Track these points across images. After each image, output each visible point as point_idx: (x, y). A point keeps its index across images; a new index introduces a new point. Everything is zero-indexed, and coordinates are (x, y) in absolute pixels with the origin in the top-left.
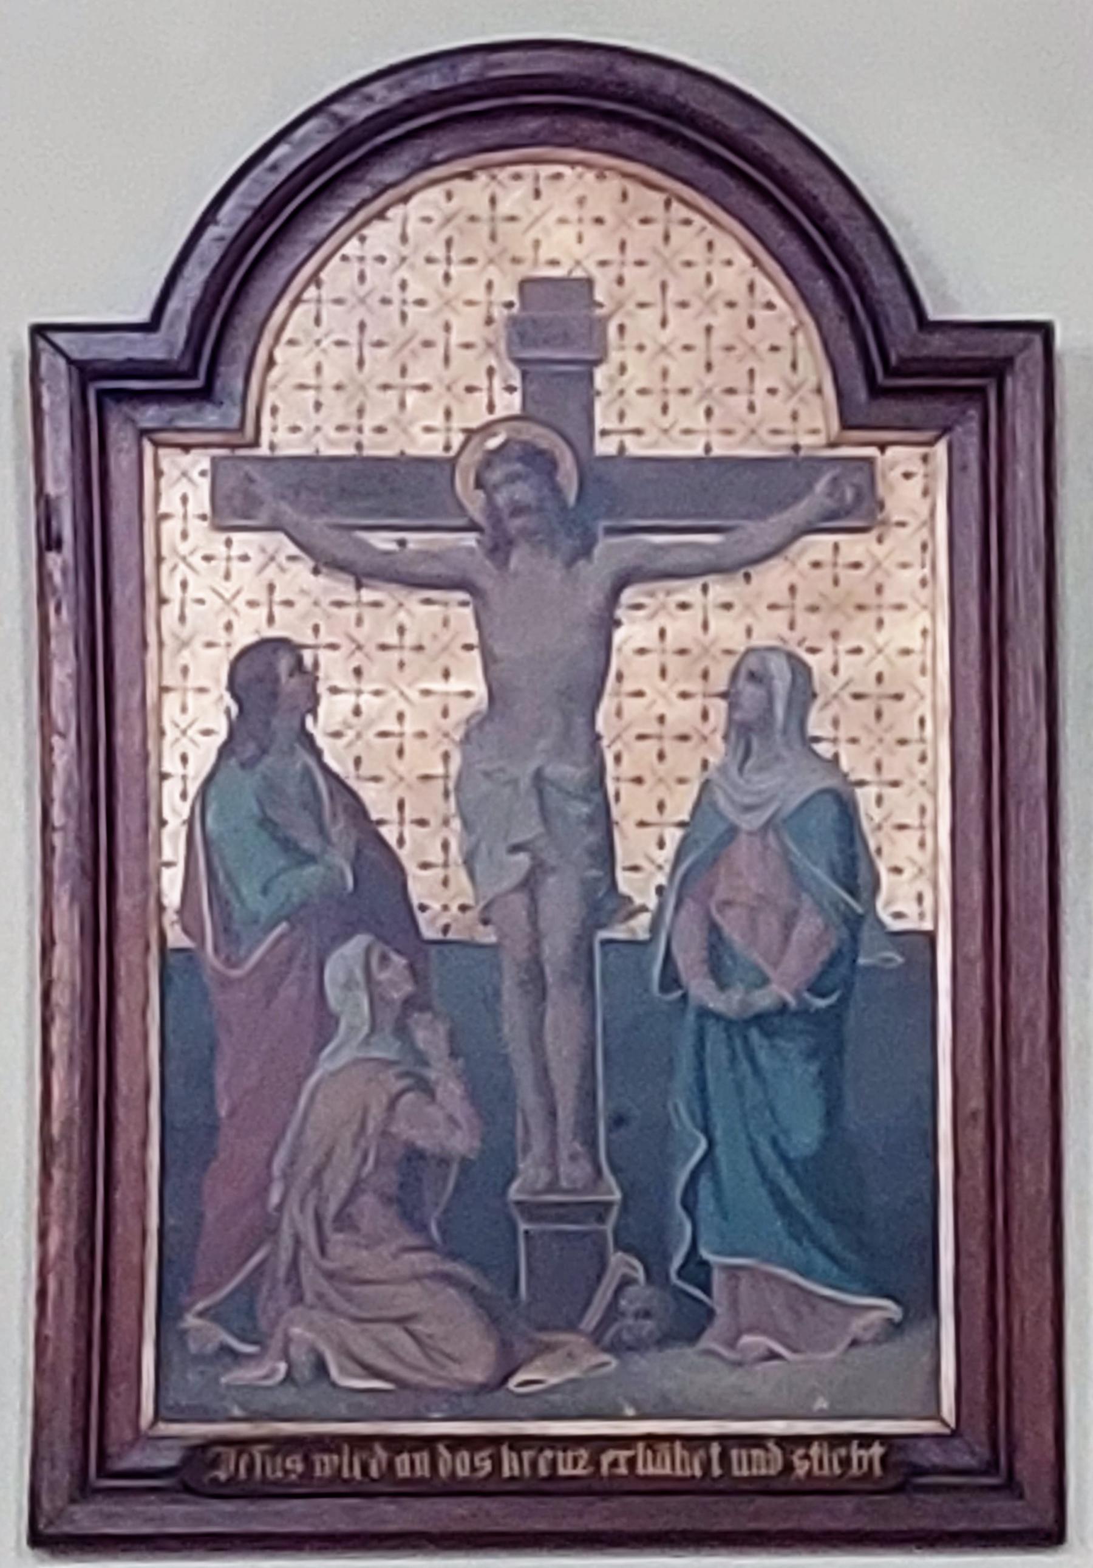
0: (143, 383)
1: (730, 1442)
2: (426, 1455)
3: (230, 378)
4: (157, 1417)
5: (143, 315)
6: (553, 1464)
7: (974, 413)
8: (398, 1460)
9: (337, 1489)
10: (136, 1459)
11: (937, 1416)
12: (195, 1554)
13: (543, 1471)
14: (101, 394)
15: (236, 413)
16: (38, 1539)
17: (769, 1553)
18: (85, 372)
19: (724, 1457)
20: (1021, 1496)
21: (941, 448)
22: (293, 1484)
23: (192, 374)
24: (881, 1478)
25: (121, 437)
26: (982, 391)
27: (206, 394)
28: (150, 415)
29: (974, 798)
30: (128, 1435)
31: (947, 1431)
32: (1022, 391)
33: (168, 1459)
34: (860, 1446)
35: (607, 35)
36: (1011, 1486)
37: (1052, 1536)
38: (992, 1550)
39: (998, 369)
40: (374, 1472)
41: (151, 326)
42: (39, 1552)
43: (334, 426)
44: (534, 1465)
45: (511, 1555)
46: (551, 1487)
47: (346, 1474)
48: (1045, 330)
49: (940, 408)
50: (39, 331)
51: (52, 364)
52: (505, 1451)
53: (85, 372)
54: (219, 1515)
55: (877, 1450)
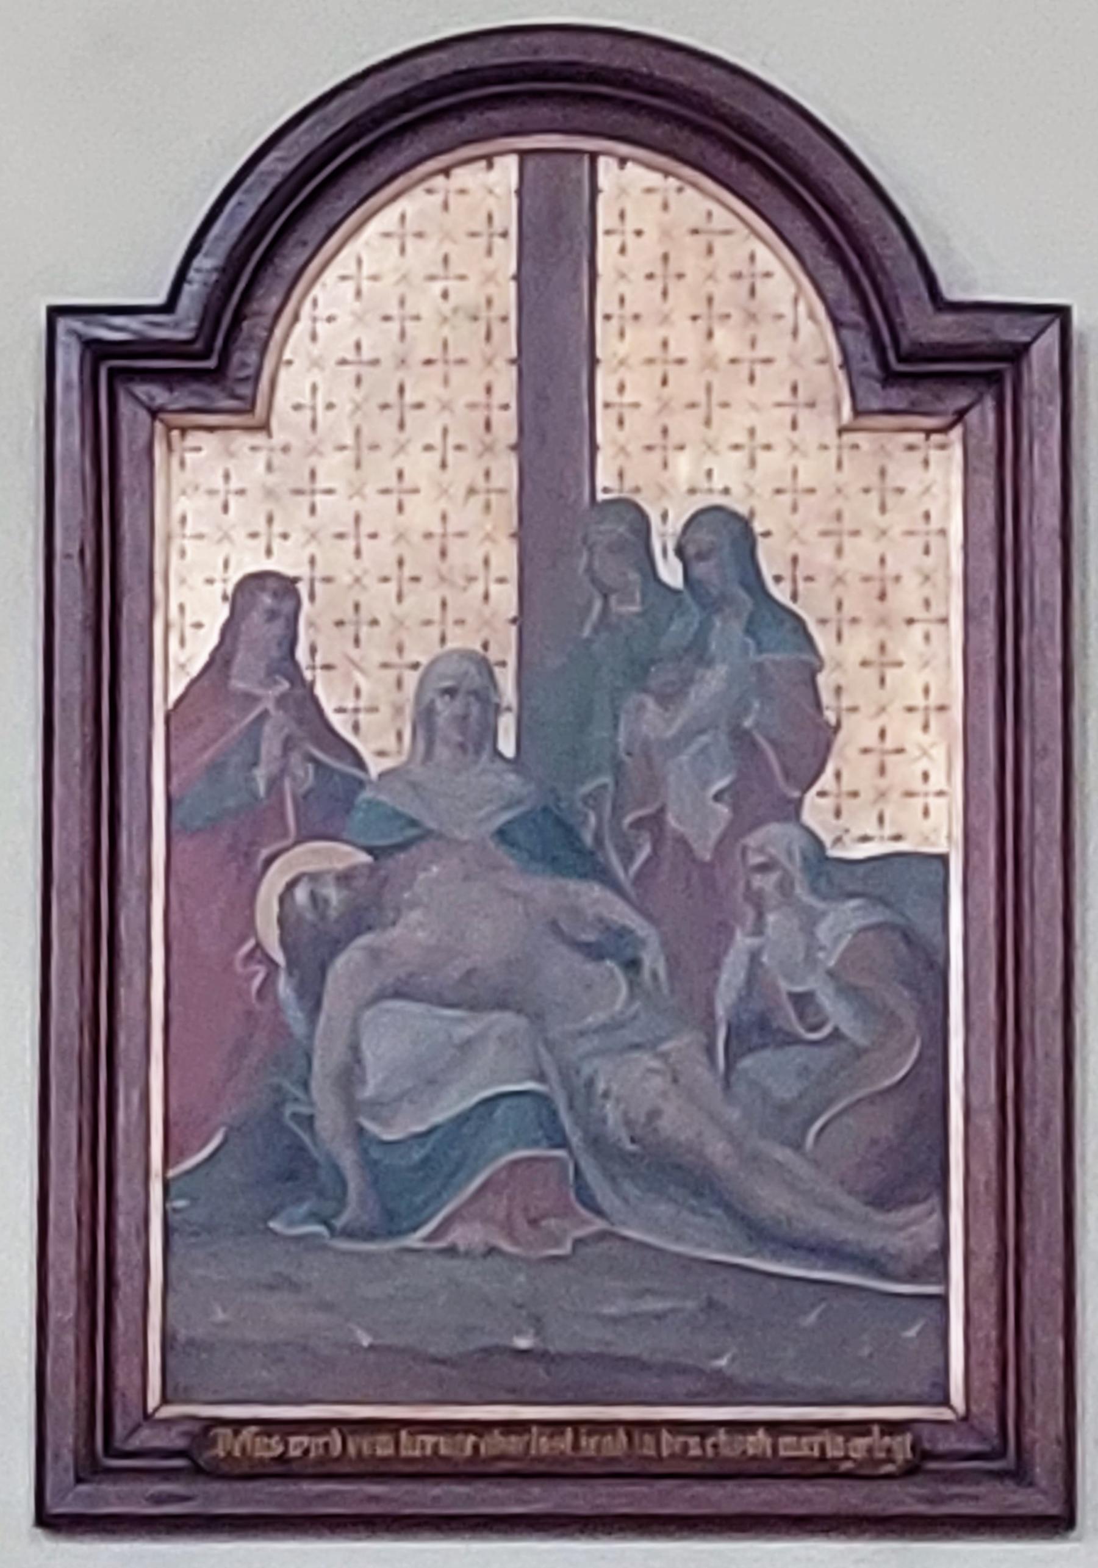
0: (170, 360)
3: (243, 357)
4: (165, 1400)
5: (159, 298)
6: (436, 1446)
7: (989, 403)
10: (146, 1438)
11: (946, 1402)
12: (983, 1534)
14: (113, 373)
15: (876, 405)
16: (46, 1520)
17: (197, 1539)
18: (95, 352)
20: (79, 1480)
21: (956, 433)
23: (205, 355)
27: (217, 376)
28: (160, 395)
29: (990, 780)
30: (137, 1415)
33: (174, 1440)
34: (883, 1433)
35: (521, 16)
36: (1020, 1474)
37: (1060, 1522)
39: (1017, 354)
41: (169, 307)
42: (39, 1531)
45: (103, 1540)
46: (824, 1470)
48: (1062, 313)
50: (55, 313)
52: (403, 1434)
53: (95, 352)
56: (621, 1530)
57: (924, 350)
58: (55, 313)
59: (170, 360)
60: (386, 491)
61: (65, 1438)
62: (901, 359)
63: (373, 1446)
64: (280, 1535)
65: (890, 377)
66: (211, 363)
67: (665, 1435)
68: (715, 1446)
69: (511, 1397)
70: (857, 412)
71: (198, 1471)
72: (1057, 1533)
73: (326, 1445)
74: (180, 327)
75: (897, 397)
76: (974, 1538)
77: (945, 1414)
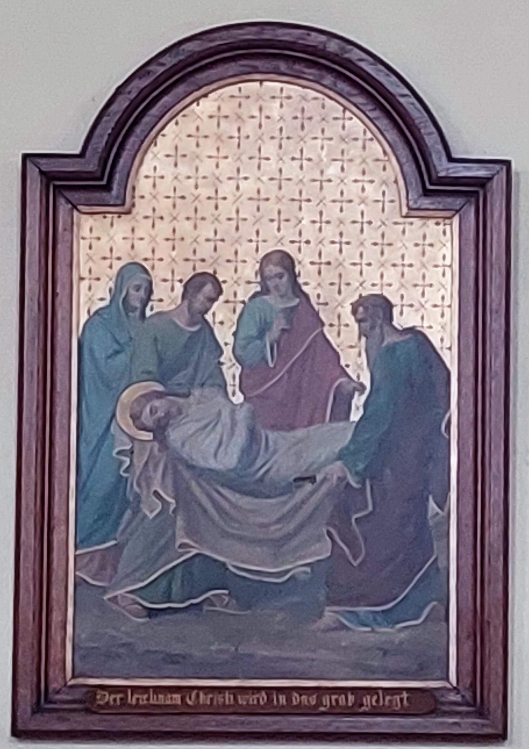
0: (82, 179)
1: (321, 692)
2: (343, 696)
4: (74, 677)
5: (77, 151)
6: (337, 701)
7: (473, 200)
8: (310, 699)
9: (335, 711)
11: (447, 679)
13: (387, 703)
16: (17, 733)
17: (245, 744)
18: (48, 177)
19: (270, 700)
22: (262, 707)
23: (101, 179)
24: (408, 707)
25: (63, 208)
26: (477, 192)
28: (74, 196)
31: (451, 687)
32: (498, 185)
33: (78, 695)
38: (245, 741)
40: (262, 703)
41: (82, 155)
42: (14, 739)
43: (299, 212)
44: (115, 700)
46: (123, 709)
47: (227, 702)
48: (507, 164)
49: (459, 202)
50: (26, 157)
51: (33, 173)
54: (93, 722)
55: (405, 695)
56: (478, 742)
57: (445, 183)
58: (26, 157)
59: (82, 179)
60: (375, 244)
61: (26, 692)
62: (431, 184)
63: (148, 699)
64: (29, 741)
65: (427, 193)
66: (104, 182)
67: (295, 694)
68: (138, 699)
69: (384, 676)
70: (410, 208)
71: (88, 711)
72: (499, 741)
73: (258, 700)
74: (91, 165)
75: (426, 202)
76: (260, 743)
77: (448, 685)
